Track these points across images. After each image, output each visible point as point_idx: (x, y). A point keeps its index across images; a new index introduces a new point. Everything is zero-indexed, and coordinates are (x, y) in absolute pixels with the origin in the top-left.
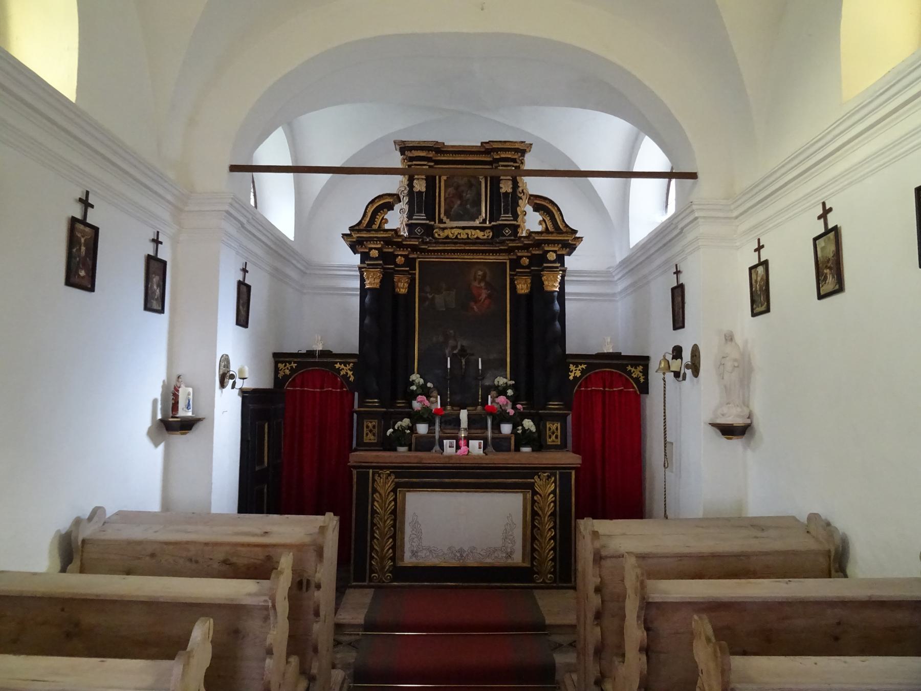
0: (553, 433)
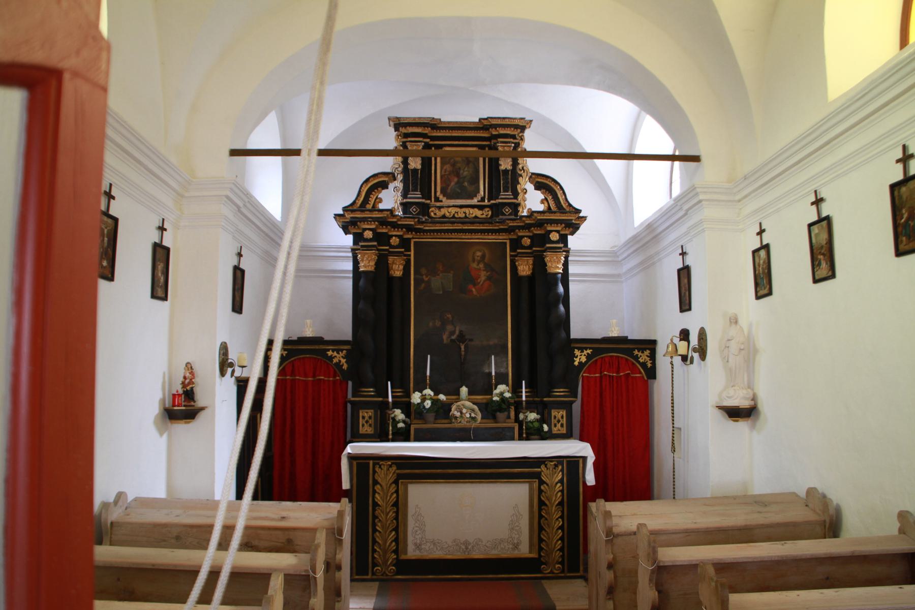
0: (559, 421)
